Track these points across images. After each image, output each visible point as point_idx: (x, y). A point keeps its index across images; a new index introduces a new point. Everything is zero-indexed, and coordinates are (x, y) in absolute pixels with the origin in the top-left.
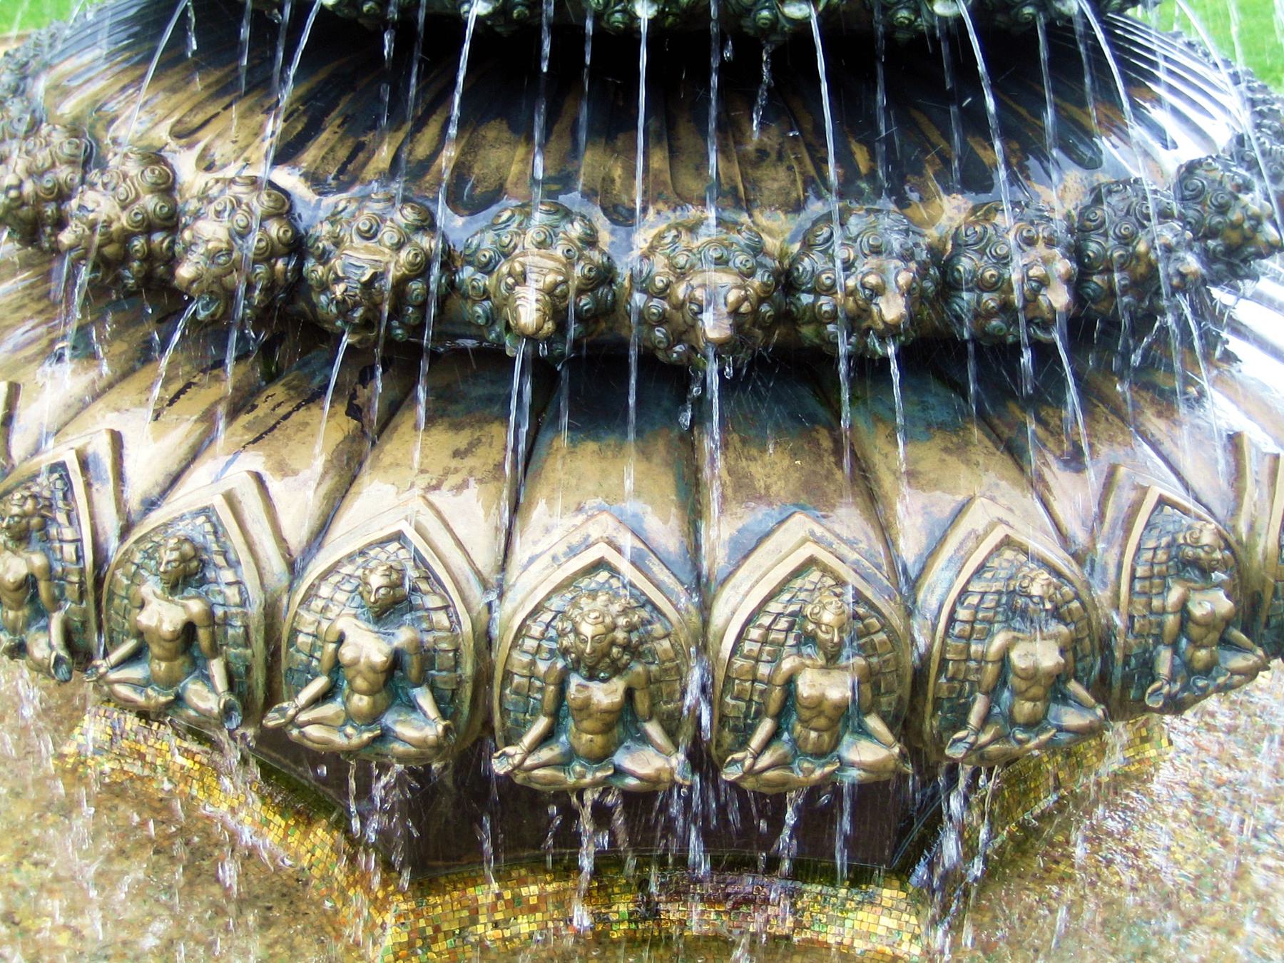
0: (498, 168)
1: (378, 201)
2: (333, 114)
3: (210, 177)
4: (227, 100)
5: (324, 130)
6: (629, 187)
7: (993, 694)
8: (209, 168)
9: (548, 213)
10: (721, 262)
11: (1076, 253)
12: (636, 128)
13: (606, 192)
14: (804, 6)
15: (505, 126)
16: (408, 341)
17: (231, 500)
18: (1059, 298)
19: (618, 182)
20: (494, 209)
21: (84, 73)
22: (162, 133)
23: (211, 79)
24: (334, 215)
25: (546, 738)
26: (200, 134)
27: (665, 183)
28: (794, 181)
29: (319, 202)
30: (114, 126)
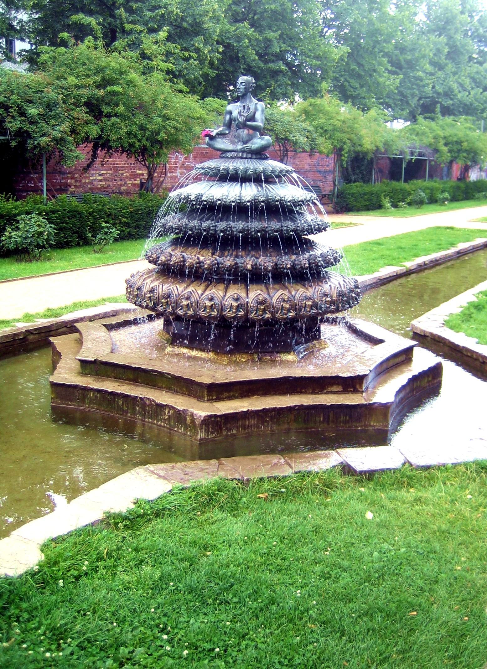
7: (305, 308)
10: (269, 262)
11: (309, 261)
17: (374, 182)
18: (307, 265)
25: (256, 314)
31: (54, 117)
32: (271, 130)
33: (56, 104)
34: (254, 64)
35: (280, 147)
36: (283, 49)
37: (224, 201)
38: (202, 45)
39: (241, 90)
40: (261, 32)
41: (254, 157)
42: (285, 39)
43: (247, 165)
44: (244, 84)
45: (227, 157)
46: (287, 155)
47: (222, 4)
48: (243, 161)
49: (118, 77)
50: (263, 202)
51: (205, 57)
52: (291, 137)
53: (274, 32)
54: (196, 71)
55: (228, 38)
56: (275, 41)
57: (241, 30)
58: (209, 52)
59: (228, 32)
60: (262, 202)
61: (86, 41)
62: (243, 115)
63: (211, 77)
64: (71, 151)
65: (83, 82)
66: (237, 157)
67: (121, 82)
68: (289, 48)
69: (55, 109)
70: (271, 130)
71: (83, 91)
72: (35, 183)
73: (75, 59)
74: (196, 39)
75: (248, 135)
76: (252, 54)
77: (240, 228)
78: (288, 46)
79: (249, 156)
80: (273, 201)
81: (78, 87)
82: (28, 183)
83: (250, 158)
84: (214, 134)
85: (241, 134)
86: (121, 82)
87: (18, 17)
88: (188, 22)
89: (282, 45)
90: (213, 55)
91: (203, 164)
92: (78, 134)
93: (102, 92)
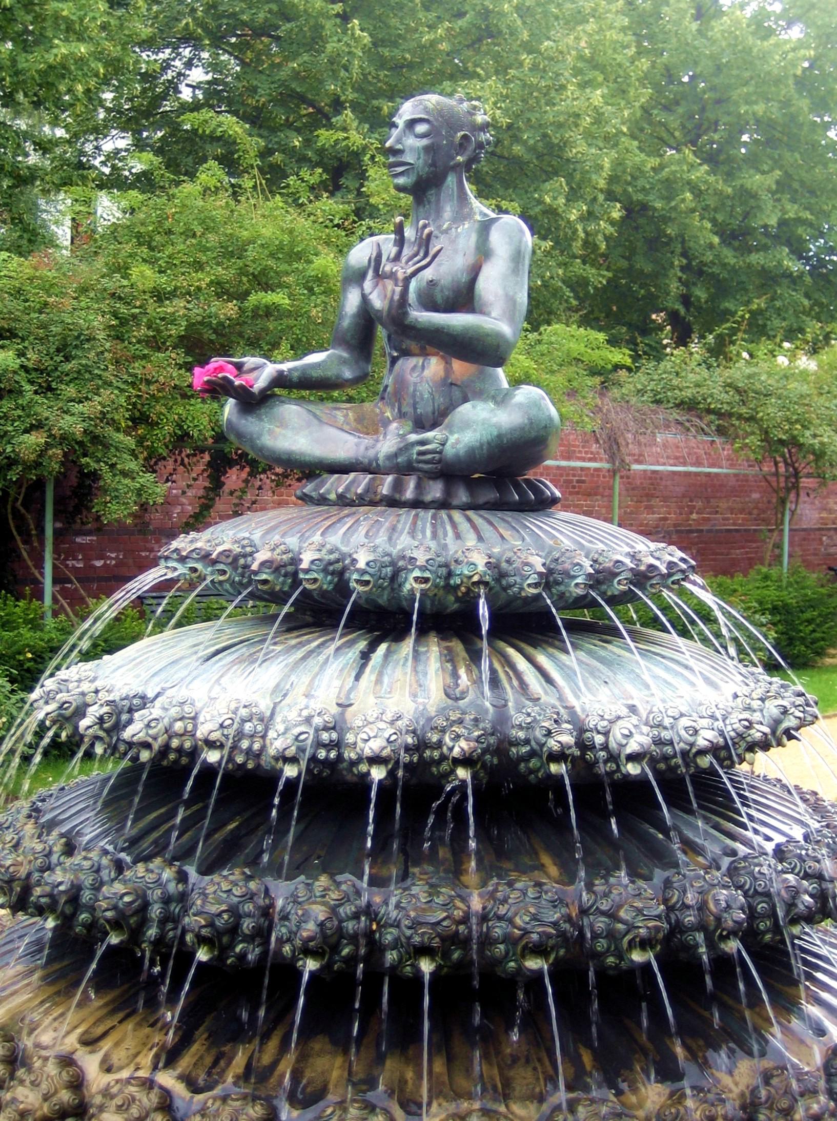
0: (323, 1073)
1: (237, 1100)
2: (202, 1029)
3: (110, 1078)
4: (121, 1015)
5: (195, 1041)
6: (418, 1086)
8: (109, 1070)
9: (360, 1109)
12: (422, 1040)
13: (402, 1091)
14: (539, 961)
15: (327, 1039)
16: (112, 929)
19: (410, 1082)
20: (321, 1104)
21: (9, 986)
22: (72, 1041)
23: (108, 998)
24: (203, 1109)
26: (101, 1043)
27: (443, 1083)
28: (538, 1079)
29: (192, 1098)
30: (36, 1032)
31: (77, 377)
32: (751, 419)
33: (87, 339)
34: (709, 257)
35: (776, 464)
36: (791, 215)
37: (249, 752)
38: (562, 201)
39: (409, 158)
40: (729, 176)
41: (462, 496)
42: (796, 191)
43: (404, 542)
44: (421, 128)
45: (322, 501)
46: (796, 487)
47: (623, 103)
48: (389, 517)
49: (284, 267)
50: (466, 761)
51: (570, 232)
52: (807, 438)
53: (763, 173)
54: (549, 268)
55: (643, 189)
56: (765, 196)
57: (673, 168)
58: (582, 219)
59: (639, 170)
60: (457, 762)
61: (203, 177)
62: (392, 276)
63: (595, 288)
64: (125, 474)
65: (182, 282)
66: (368, 500)
67: (290, 279)
68: (807, 215)
69: (79, 353)
70: (751, 419)
71: (176, 307)
72: (87, 559)
73: (167, 224)
74: (547, 186)
75: (447, 384)
76: (702, 228)
77: (310, 928)
78: (806, 209)
79: (435, 491)
80: (533, 754)
81: (160, 296)
82: (66, 559)
83: (444, 504)
84: (260, 382)
85: (412, 378)
86: (290, 279)
87: (104, 148)
88: (525, 143)
89: (788, 206)
90: (592, 227)
91: (207, 534)
92: (154, 425)
93: (230, 309)
